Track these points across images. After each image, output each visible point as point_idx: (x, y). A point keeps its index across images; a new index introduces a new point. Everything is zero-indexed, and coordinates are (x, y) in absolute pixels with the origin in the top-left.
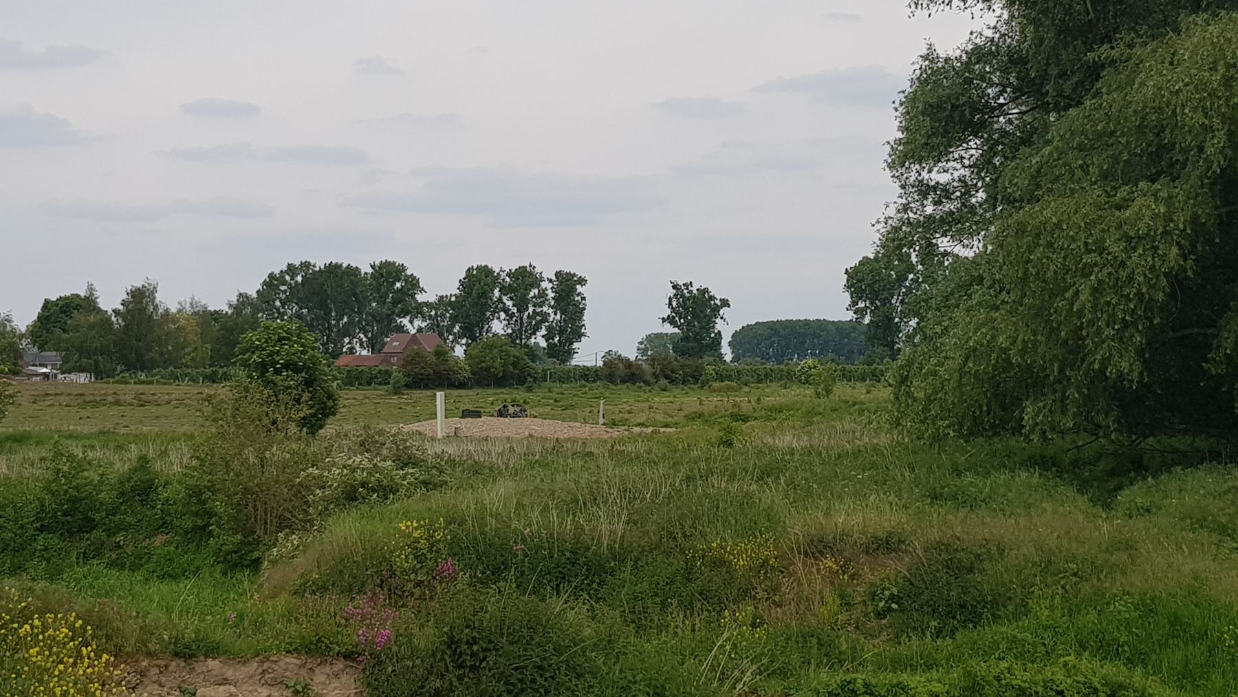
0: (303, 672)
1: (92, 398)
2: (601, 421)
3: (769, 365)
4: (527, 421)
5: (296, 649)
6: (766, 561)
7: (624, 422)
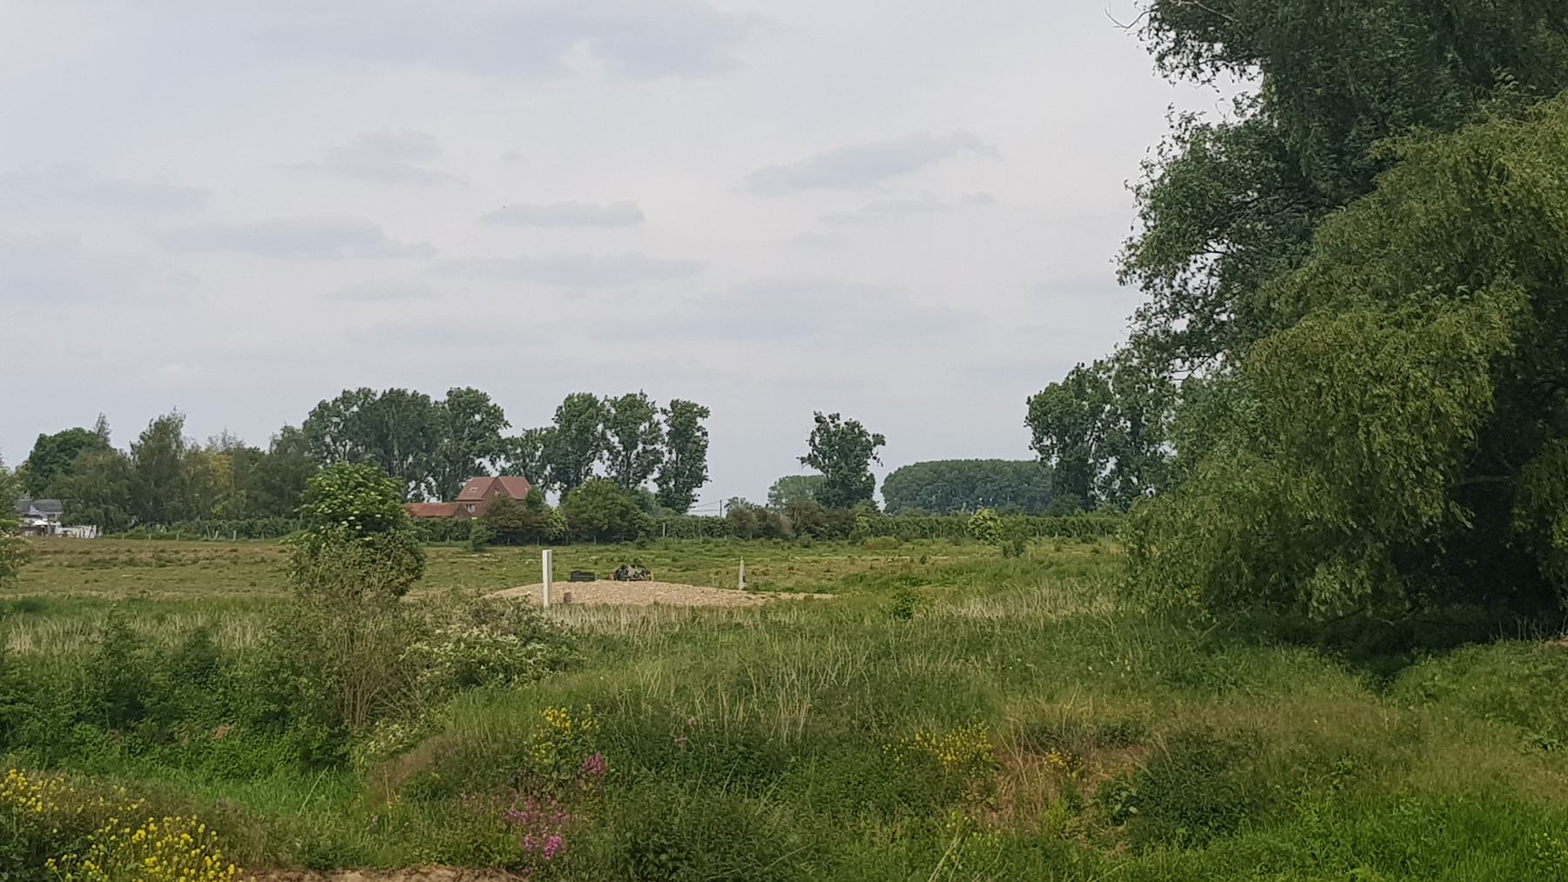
1: (100, 556)
2: (742, 585)
3: (934, 516)
4: (650, 585)
5: (449, 859)
6: (979, 755)
7: (768, 587)
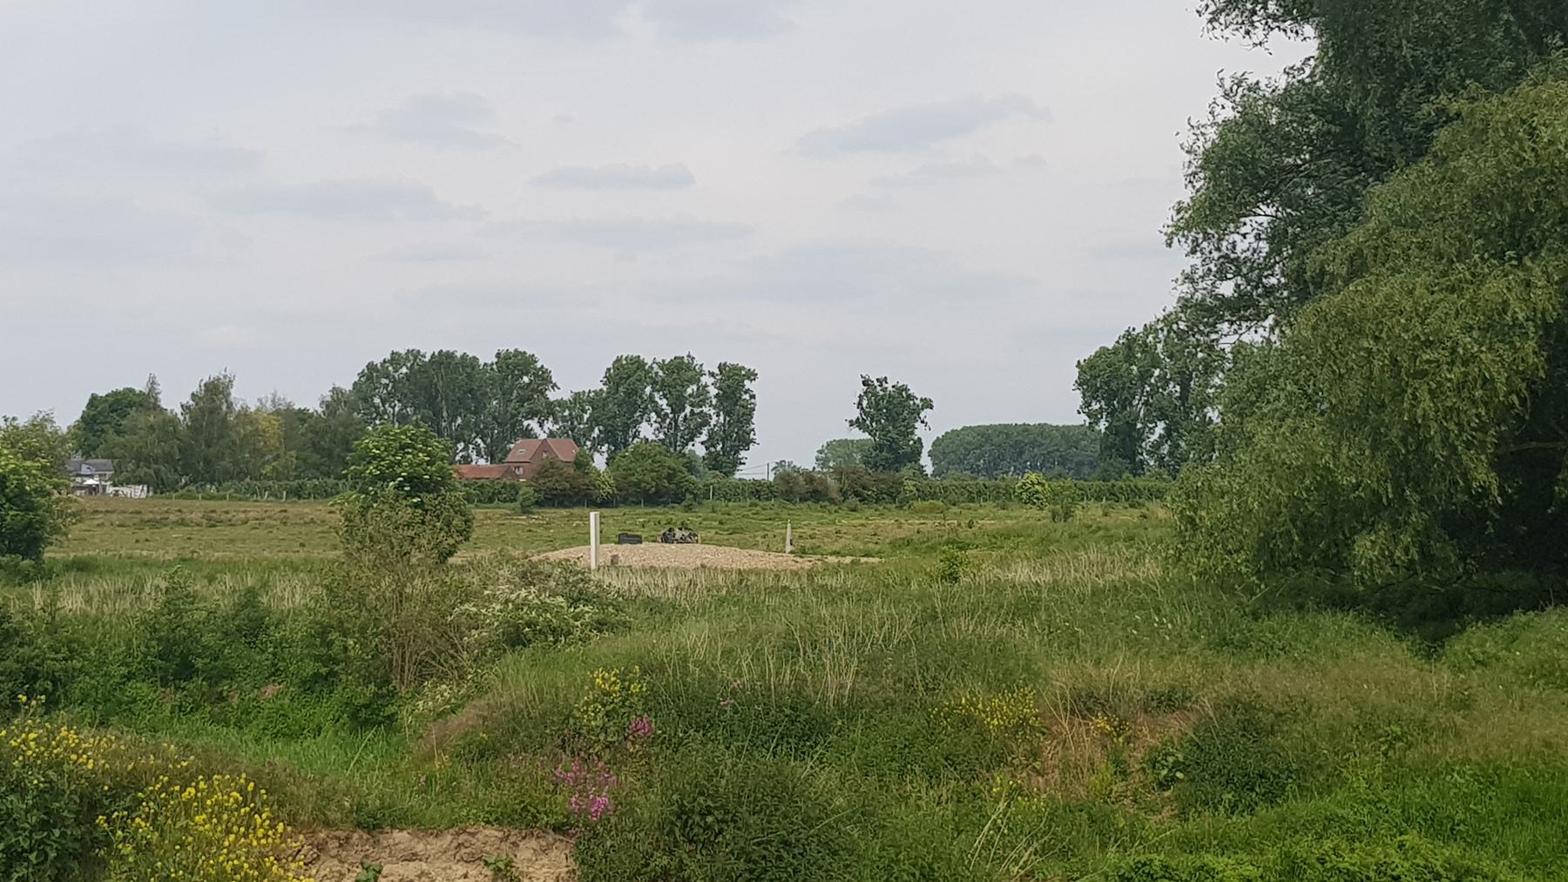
0: (504, 846)
2: (789, 548)
4: (698, 548)
6: (1025, 719)
7: (814, 550)
